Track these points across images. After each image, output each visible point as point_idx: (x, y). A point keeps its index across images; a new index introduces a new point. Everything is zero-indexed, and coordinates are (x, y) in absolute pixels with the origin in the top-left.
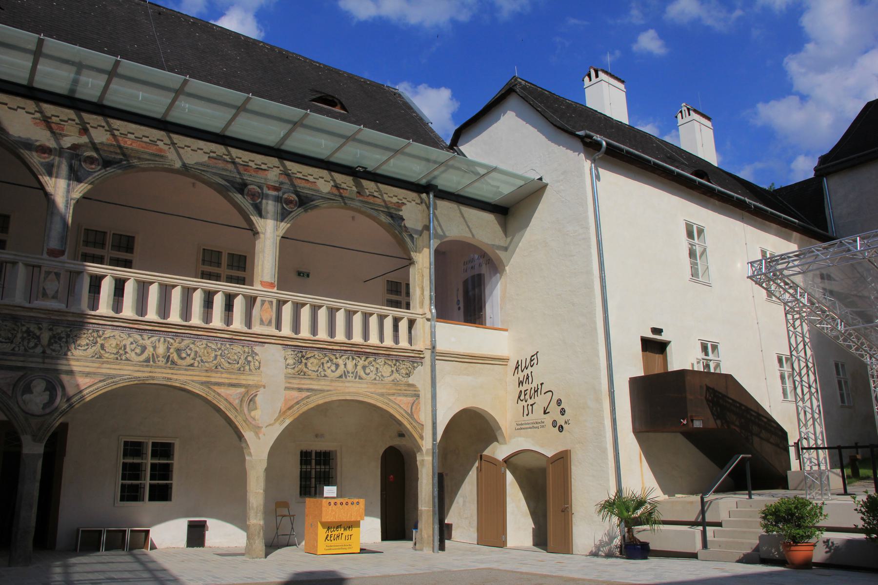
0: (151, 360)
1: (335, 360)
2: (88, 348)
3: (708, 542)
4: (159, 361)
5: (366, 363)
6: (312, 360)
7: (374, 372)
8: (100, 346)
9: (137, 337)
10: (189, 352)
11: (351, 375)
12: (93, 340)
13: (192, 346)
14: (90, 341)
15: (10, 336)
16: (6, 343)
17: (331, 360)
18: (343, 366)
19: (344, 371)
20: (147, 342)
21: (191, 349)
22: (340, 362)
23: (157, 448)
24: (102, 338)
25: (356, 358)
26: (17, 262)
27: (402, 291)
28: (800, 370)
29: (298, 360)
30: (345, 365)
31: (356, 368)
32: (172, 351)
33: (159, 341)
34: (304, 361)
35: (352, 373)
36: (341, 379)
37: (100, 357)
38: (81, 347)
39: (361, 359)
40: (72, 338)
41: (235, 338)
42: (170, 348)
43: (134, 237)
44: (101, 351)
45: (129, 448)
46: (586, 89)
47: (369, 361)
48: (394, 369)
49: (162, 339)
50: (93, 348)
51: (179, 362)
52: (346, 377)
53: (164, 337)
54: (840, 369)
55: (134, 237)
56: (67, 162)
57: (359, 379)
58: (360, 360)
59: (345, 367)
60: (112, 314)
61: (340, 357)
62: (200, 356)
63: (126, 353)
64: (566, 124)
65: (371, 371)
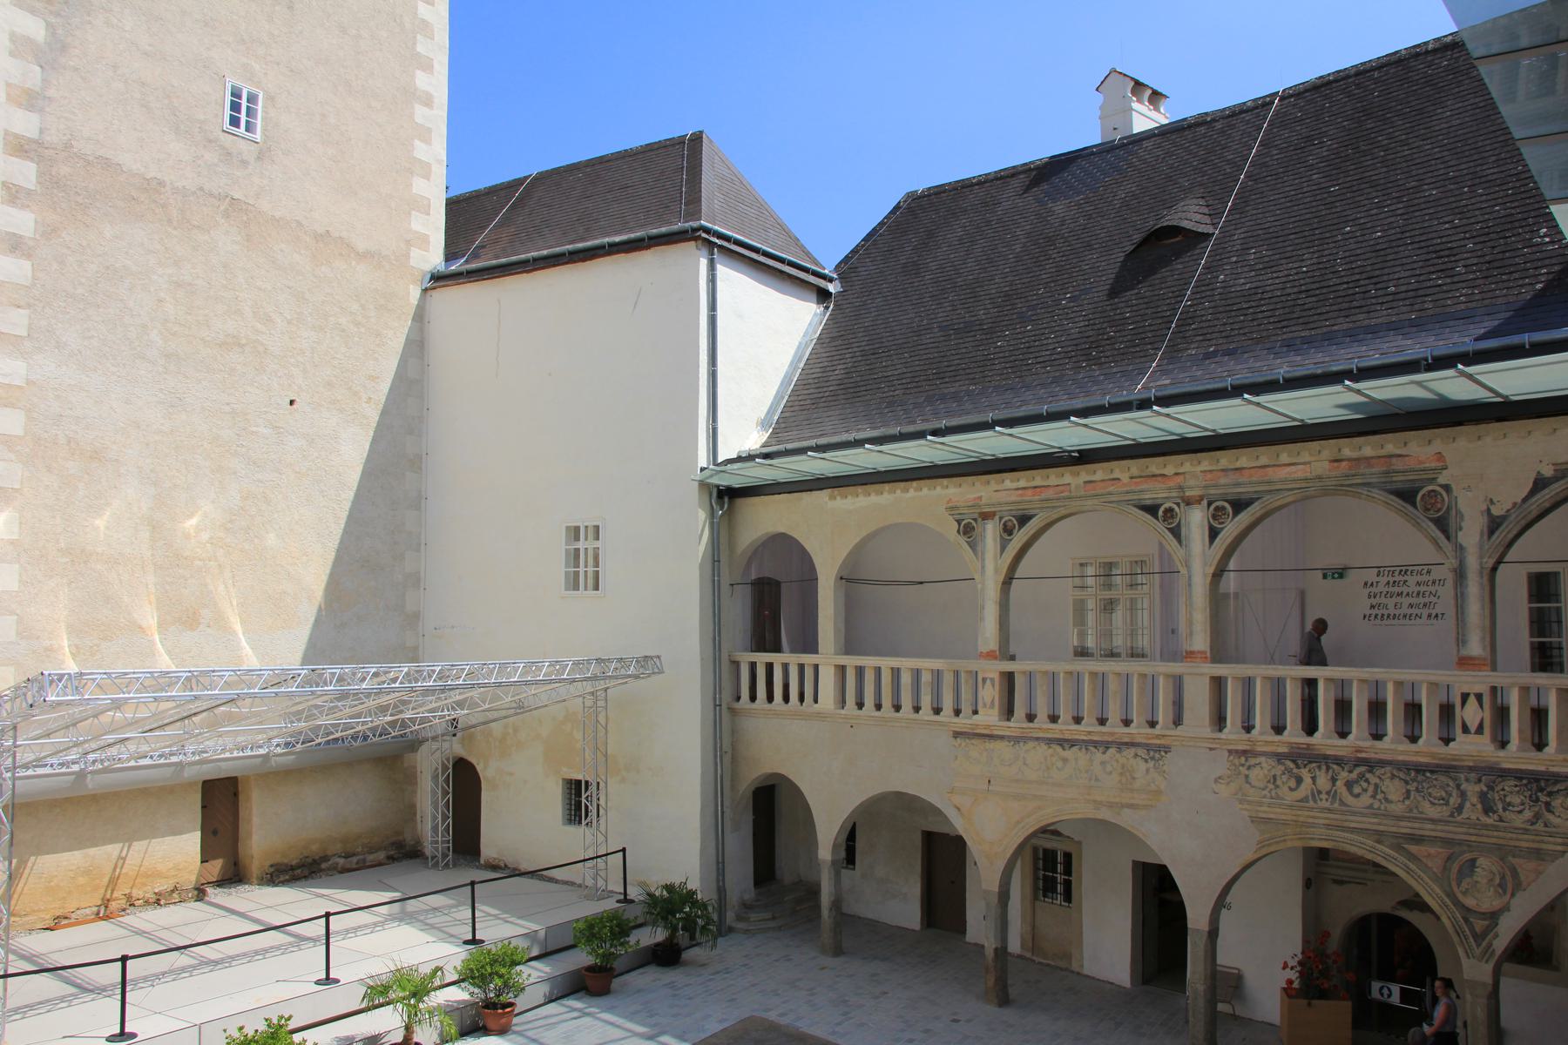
2: (1524, 809)
3: (1189, 932)
4: (1321, 800)
5: (1354, 775)
6: (1256, 771)
7: (1370, 792)
9: (1059, 749)
10: (1365, 785)
11: (1324, 796)
12: (1235, 770)
13: (1368, 775)
14: (1526, 797)
15: (1444, 794)
16: (1440, 805)
21: (1367, 781)
22: (1304, 773)
24: (1545, 792)
25: (1091, 748)
28: (1291, 275)
29: (1530, 796)
30: (1314, 778)
31: (1334, 785)
32: (1339, 783)
34: (1543, 798)
36: (1307, 805)
38: (1513, 806)
40: (1497, 792)
42: (1337, 780)
50: (1533, 809)
56: (703, 510)
57: (1340, 805)
59: (1314, 783)
61: (1305, 766)
62: (1382, 792)
63: (1277, 787)
64: (541, 671)
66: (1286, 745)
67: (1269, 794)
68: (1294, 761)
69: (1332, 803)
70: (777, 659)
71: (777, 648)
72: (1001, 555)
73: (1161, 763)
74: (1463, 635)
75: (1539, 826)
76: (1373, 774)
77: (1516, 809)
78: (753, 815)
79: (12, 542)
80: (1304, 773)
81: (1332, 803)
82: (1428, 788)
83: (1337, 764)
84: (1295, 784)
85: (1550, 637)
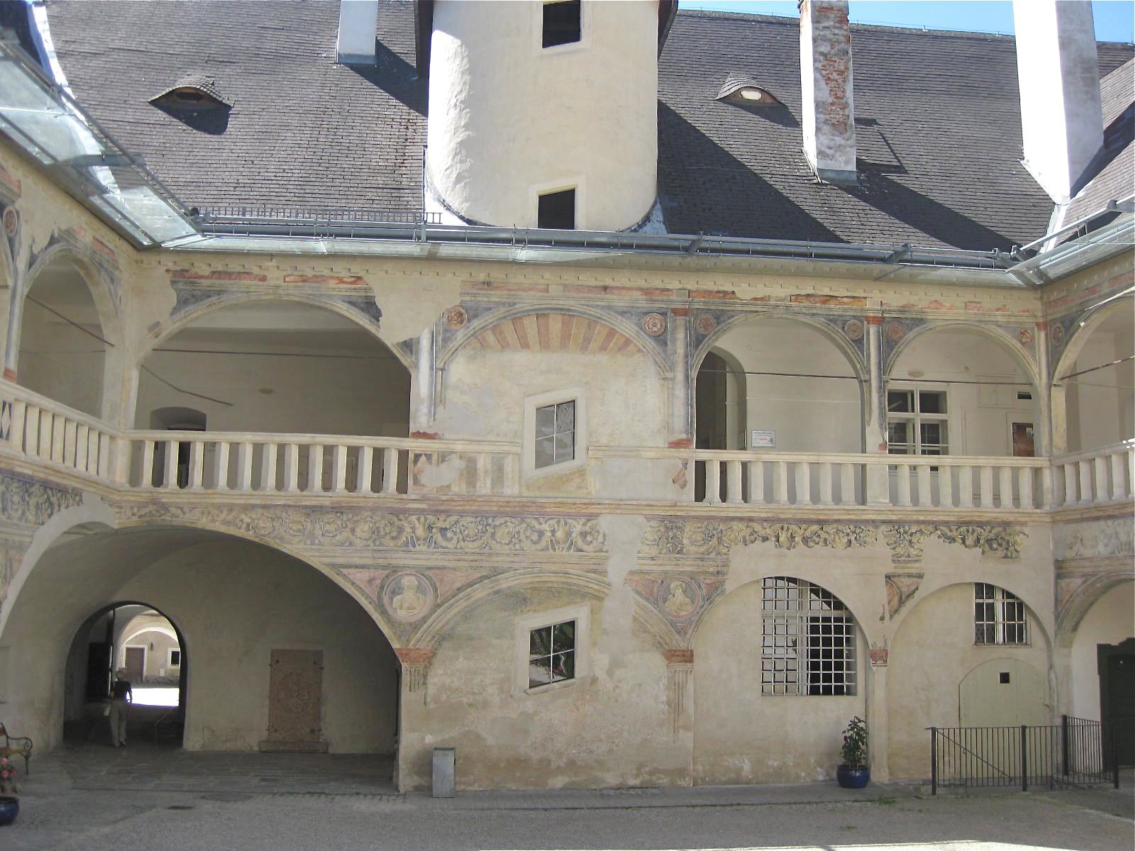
0: (550, 547)
8: (490, 534)
13: (819, 532)
17: (48, 498)
18: (549, 534)
19: (552, 540)
20: (545, 527)
35: (424, 540)
37: (351, 544)
38: (329, 533)
39: (578, 523)
41: (338, 509)
43: (946, 421)
44: (909, 548)
45: (833, 648)
47: (591, 525)
48: (853, 538)
49: (562, 522)
51: (585, 547)
52: (414, 546)
54: (843, 344)
55: (946, 421)
58: (576, 525)
59: (553, 536)
60: (933, 508)
63: (520, 541)
66: (1049, 515)
67: (513, 548)
68: (398, 517)
69: (429, 547)
70: (725, 455)
71: (721, 445)
72: (842, 241)
73: (862, 535)
74: (432, 376)
75: (486, 550)
76: (246, 514)
77: (699, 544)
78: (1120, 644)
79: (85, 245)
80: (545, 527)
81: (429, 547)
82: (289, 523)
83: (979, 527)
84: (537, 538)
85: (714, 369)
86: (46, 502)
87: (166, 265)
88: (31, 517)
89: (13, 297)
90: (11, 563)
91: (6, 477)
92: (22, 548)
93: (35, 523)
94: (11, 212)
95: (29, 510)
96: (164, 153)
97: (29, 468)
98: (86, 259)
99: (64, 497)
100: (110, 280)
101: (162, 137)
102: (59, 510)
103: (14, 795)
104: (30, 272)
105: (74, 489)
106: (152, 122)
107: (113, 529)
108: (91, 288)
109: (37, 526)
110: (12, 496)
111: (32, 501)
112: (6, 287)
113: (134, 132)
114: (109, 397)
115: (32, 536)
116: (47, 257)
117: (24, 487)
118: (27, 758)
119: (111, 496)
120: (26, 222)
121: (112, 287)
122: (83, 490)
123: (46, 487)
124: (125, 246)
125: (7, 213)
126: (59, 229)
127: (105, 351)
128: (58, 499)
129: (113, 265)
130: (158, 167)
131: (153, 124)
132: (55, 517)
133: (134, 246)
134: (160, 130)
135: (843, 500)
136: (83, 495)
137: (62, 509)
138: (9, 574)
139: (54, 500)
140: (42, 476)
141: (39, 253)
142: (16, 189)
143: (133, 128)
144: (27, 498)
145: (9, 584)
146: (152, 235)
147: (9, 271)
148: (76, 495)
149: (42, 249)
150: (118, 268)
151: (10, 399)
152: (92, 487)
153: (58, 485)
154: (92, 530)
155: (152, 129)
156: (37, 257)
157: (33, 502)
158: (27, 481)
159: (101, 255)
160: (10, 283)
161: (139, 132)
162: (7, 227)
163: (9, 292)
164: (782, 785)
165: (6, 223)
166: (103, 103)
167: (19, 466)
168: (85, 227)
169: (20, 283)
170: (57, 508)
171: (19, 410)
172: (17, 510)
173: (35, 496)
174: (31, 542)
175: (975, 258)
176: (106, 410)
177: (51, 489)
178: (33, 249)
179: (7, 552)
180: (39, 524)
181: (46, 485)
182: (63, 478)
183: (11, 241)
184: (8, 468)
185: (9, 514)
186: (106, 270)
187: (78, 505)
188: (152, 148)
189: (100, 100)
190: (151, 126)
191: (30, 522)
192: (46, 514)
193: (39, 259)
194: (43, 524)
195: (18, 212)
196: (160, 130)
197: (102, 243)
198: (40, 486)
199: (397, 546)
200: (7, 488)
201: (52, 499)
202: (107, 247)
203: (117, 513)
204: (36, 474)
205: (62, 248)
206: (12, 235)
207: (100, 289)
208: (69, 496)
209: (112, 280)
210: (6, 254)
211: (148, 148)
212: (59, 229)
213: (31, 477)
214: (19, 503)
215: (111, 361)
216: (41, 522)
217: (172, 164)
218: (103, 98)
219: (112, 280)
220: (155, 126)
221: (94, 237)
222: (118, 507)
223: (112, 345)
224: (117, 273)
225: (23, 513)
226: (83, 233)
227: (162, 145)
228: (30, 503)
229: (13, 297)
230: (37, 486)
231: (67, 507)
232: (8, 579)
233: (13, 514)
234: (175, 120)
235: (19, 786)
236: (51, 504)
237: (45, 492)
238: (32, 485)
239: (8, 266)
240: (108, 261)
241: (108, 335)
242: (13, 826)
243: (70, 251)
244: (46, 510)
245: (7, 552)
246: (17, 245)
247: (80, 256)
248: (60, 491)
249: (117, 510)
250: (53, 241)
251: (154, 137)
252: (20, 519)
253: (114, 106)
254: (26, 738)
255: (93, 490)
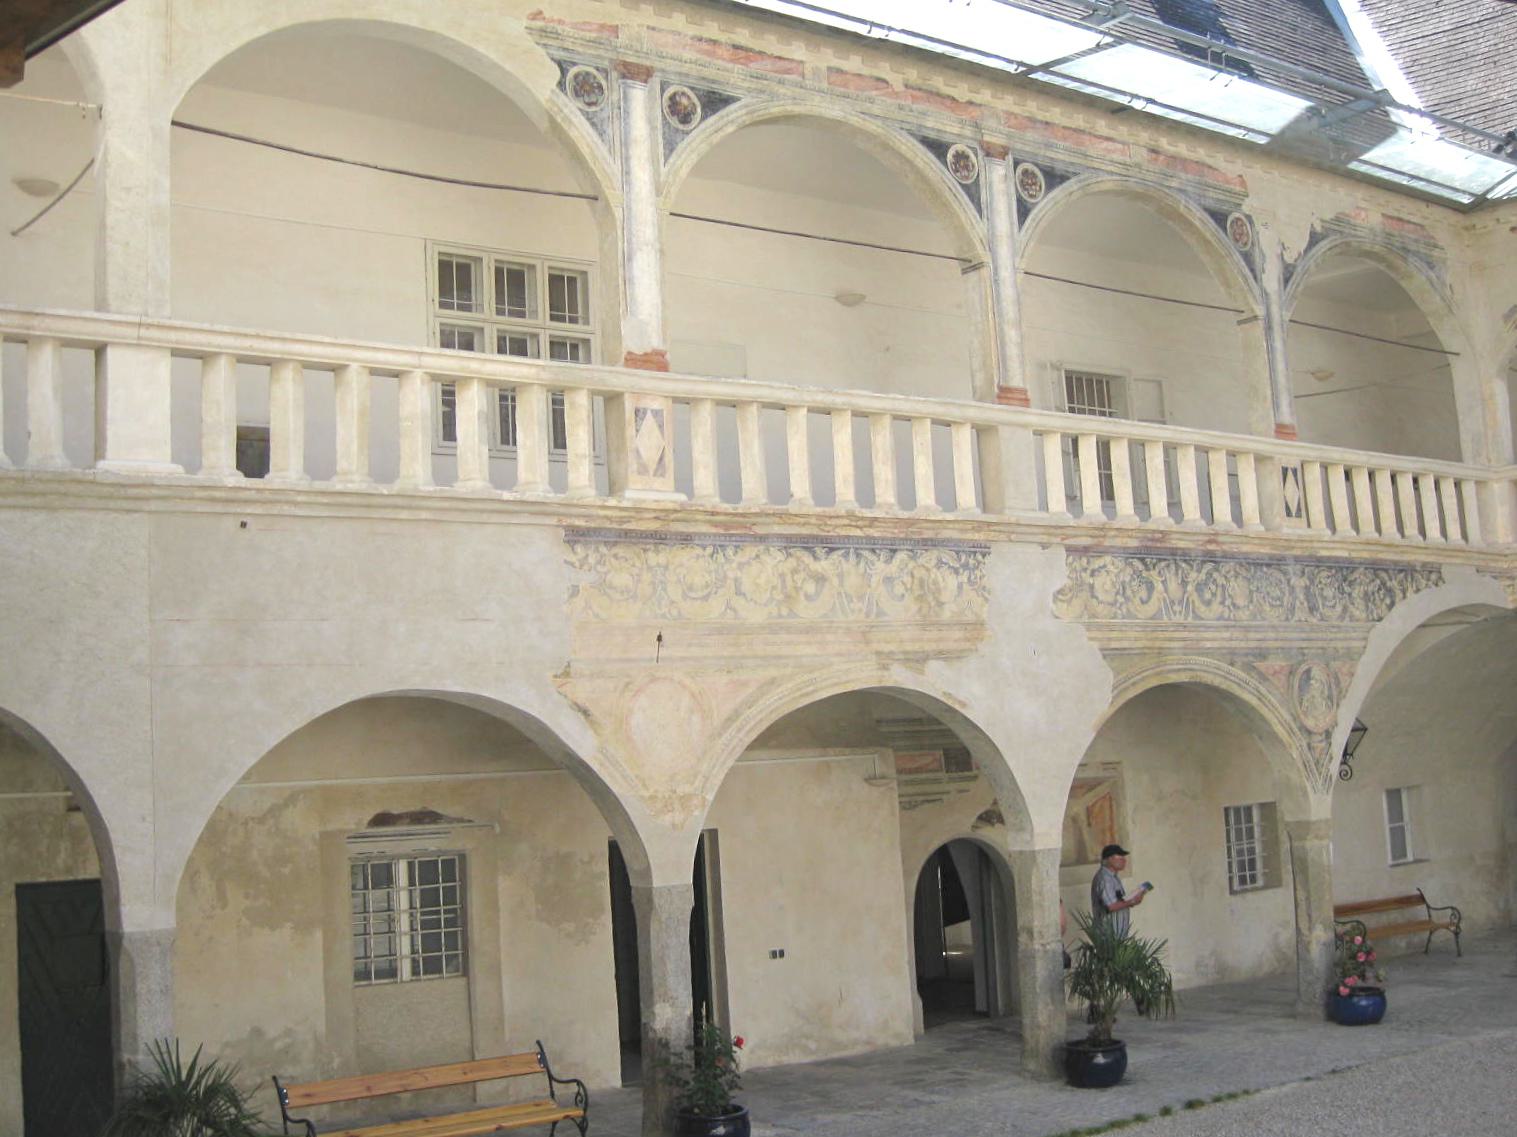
1: (1145, 574)
11: (1177, 608)
17: (1383, 584)
23: (1244, 830)
26: (346, 366)
27: (540, 309)
30: (841, 576)
33: (1406, 578)
46: (1273, 132)
53: (857, 549)
57: (1351, 620)
65: (907, 590)
86: (1379, 589)
87: (1508, 222)
88: (1358, 612)
89: (1269, 328)
90: (1337, 678)
91: (1307, 566)
92: (1352, 656)
93: (1368, 620)
94: (1238, 219)
95: (1353, 604)
96: (1496, 59)
97: (1342, 549)
98: (1377, 248)
99: (1409, 579)
100: (1426, 266)
101: (1492, 37)
102: (1404, 597)
103: (1379, 985)
104: (1288, 289)
105: (1424, 565)
106: (1477, 20)
107: (1507, 610)
108: (1404, 284)
109: (1370, 624)
110: (1322, 589)
111: (1356, 591)
112: (1255, 318)
113: (1453, 43)
114: (1469, 425)
115: (1365, 639)
116: (1312, 261)
117: (1340, 575)
118: (1456, 934)
119: (1493, 564)
120: (1265, 225)
121: (1432, 275)
122: (1441, 564)
123: (1375, 570)
124: (1437, 212)
125: (1233, 222)
126: (1322, 221)
127: (1449, 365)
128: (1401, 583)
129: (1428, 245)
130: (1489, 83)
131: (1478, 22)
132: (1399, 608)
133: (1455, 210)
134: (1490, 27)
135: (878, 500)
136: (1442, 571)
137: (1408, 594)
138: (1335, 693)
139: (1393, 584)
140: (1365, 555)
141: (1296, 260)
142: (1238, 189)
143: (1450, 38)
144: (1347, 589)
145: (1338, 705)
146: (1472, 191)
147: (1254, 297)
148: (1431, 572)
149: (1300, 254)
150: (1436, 246)
151: (1294, 463)
152: (1457, 557)
153: (1396, 563)
154: (1478, 616)
155: (1479, 30)
156: (1294, 267)
157: (1357, 592)
158: (1342, 565)
159: (1401, 236)
160: (1260, 311)
161: (1460, 41)
162: (1237, 241)
163: (1261, 323)
164: (402, 900)
165: (1234, 234)
166: (1407, 18)
167: (1323, 548)
168: (1363, 204)
169: (1275, 309)
170: (1401, 595)
171: (1314, 474)
172: (1334, 607)
173: (1361, 584)
174: (1365, 647)
175: (721, 134)
176: (1467, 446)
177: (1386, 571)
178: (1285, 257)
179: (1327, 665)
180: (1373, 620)
181: (1375, 567)
182: (1402, 552)
183: (1248, 258)
184: (1307, 554)
185: (1321, 614)
186: (1416, 254)
187: (1437, 585)
188: (1478, 58)
189: (1403, 14)
190: (1476, 25)
191: (1358, 620)
192: (1384, 606)
193: (1299, 269)
194: (1380, 619)
195: (1249, 217)
196: (1490, 27)
197: (1400, 220)
198: (1366, 569)
199: (939, 625)
200: (1312, 581)
201: (1389, 584)
202: (1409, 222)
203: (1509, 586)
204: (1354, 555)
205: (1334, 243)
206: (1247, 248)
207: (1416, 283)
208: (1417, 575)
209: (1431, 265)
210: (1244, 277)
211: (1473, 59)
212: (1322, 221)
213: (1350, 561)
214: (1334, 598)
215: (1460, 372)
216: (1376, 617)
217: (1508, 72)
218: (1406, 10)
219: (1431, 265)
220: (1481, 24)
221: (1383, 215)
222: (1509, 578)
223: (1457, 354)
224: (1436, 253)
225: (1345, 609)
226: (1363, 214)
227: (1493, 48)
228: (1354, 595)
229: (1269, 328)
230: (1362, 569)
231: (1418, 590)
232: (1335, 701)
233: (1327, 612)
234: (1509, 5)
235: (1382, 973)
236: (1390, 591)
237: (1377, 576)
238: (1354, 570)
239: (1251, 290)
240: (1416, 241)
241: (1449, 342)
242: (1380, 1026)
243: (1348, 244)
244: (1382, 600)
245: (1327, 665)
246: (1258, 259)
247: (1367, 247)
248: (1401, 571)
249: (1508, 582)
250: (1314, 239)
251: (1481, 40)
252: (1342, 618)
253: (1423, 16)
254: (1452, 908)
255: (1458, 561)
